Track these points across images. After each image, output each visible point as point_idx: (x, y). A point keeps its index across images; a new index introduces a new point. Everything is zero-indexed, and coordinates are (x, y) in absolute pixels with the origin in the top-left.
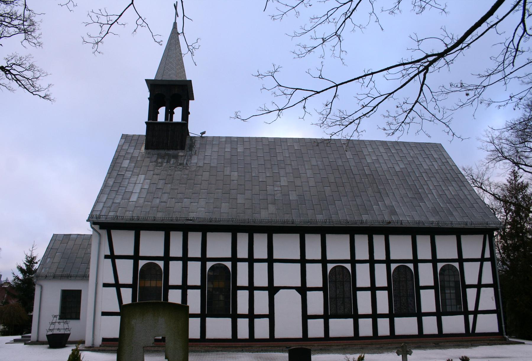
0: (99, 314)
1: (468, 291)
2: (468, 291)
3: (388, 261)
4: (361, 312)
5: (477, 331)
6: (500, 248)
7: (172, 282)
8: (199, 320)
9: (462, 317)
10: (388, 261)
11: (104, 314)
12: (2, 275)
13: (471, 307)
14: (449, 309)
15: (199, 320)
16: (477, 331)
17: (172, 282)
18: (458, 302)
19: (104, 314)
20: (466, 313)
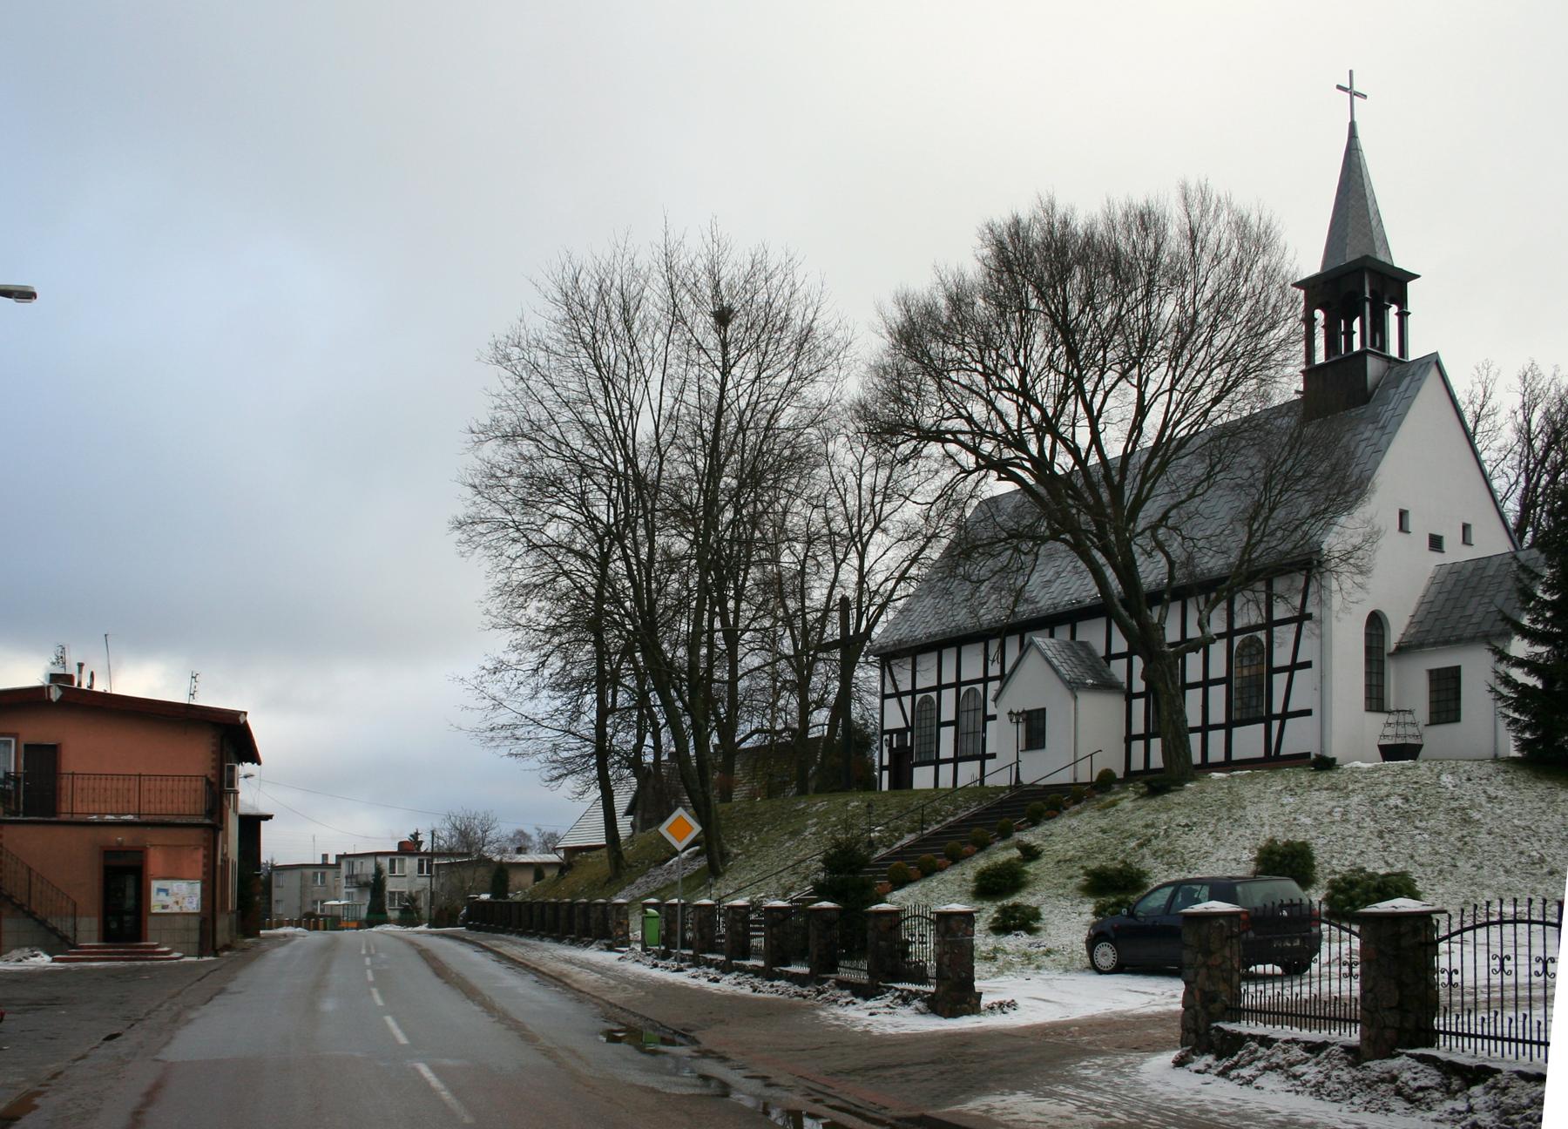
0: (1316, 712)
5: (1283, 752)
9: (1261, 726)
11: (1308, 713)
12: (1437, 353)
13: (1277, 708)
16: (1283, 752)
19: (1308, 713)
20: (1267, 719)
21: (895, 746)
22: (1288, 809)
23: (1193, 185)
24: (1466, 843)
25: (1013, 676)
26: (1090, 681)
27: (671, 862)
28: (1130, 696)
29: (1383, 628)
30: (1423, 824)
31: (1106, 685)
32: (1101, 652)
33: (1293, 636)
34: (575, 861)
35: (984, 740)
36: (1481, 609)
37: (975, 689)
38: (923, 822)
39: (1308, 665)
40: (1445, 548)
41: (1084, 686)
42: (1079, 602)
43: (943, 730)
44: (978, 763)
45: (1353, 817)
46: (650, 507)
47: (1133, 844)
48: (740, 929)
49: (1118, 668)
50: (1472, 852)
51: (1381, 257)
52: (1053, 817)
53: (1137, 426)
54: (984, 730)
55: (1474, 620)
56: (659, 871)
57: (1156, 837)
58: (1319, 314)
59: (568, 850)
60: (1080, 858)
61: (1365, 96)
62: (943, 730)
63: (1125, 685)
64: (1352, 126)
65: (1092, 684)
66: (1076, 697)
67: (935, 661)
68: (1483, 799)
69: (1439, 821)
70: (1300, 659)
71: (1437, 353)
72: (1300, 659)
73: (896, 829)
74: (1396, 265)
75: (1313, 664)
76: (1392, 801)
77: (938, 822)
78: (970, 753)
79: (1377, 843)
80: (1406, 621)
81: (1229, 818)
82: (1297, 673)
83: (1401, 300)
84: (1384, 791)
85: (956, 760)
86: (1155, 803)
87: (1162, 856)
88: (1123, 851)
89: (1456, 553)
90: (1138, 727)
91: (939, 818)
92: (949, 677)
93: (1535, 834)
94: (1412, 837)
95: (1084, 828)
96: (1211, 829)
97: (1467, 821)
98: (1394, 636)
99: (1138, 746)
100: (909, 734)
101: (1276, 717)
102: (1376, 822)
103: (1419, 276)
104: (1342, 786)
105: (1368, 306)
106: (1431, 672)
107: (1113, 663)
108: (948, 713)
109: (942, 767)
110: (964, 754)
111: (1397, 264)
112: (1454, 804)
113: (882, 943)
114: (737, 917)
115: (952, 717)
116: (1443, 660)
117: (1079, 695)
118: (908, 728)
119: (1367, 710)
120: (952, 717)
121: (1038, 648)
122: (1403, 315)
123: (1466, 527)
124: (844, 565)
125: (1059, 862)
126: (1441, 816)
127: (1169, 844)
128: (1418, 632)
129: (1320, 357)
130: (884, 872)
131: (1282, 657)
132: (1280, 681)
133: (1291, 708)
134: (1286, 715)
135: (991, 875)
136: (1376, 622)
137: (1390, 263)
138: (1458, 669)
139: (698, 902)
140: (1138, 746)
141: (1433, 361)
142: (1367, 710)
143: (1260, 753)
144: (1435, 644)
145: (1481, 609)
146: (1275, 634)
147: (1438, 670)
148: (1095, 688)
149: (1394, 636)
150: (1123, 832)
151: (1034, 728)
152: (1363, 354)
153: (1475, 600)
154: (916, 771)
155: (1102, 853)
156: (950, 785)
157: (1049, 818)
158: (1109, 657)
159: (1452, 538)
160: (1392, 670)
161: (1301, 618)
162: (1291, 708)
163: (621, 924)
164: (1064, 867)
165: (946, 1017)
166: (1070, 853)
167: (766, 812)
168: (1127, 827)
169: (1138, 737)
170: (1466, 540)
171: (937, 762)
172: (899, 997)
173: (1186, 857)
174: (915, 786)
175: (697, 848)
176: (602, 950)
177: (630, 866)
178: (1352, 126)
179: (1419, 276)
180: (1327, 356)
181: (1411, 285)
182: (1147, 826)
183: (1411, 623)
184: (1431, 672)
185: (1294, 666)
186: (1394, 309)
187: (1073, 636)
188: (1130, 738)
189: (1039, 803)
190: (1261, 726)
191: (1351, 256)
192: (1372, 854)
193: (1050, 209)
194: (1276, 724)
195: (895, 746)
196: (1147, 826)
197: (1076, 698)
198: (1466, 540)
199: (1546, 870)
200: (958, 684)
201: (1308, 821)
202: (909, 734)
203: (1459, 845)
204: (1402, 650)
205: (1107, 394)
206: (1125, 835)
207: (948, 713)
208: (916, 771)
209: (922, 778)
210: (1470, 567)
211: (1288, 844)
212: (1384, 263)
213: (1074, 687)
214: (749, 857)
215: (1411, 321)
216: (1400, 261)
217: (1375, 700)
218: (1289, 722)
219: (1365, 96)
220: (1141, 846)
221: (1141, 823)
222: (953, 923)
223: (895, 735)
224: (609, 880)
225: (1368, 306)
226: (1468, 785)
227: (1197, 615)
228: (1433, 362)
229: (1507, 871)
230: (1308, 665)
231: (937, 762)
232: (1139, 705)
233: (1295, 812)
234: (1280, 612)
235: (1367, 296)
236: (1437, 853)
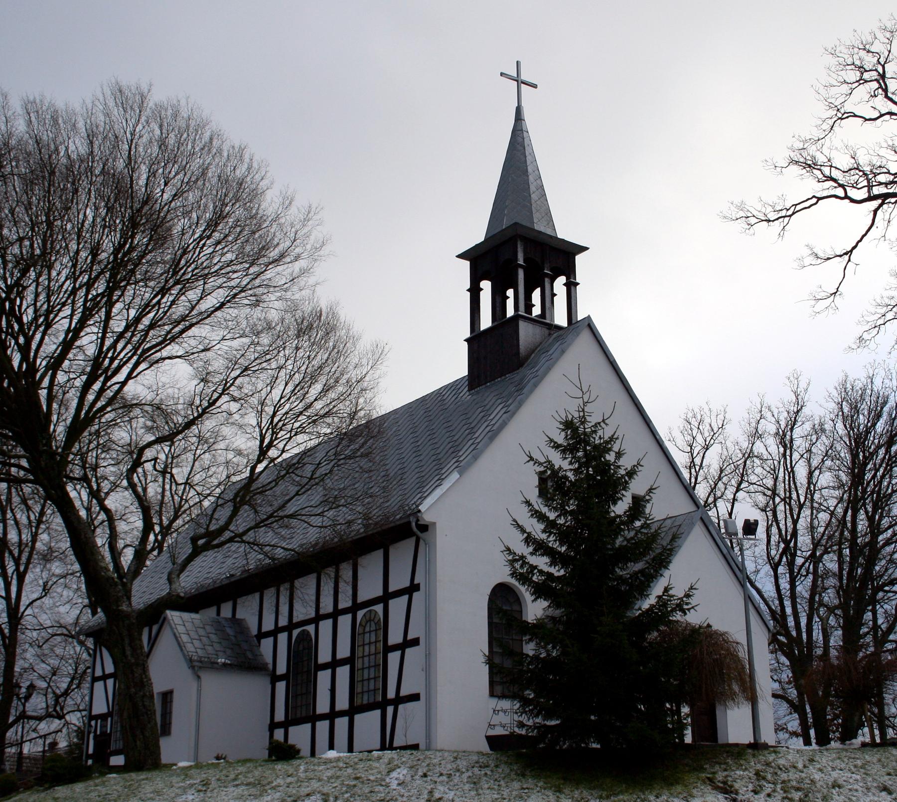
9: (378, 712)
12: (589, 317)
13: (391, 694)
21: (98, 733)
25: (153, 652)
26: (221, 660)
28: (275, 679)
29: (520, 604)
32: (254, 631)
42: (232, 576)
46: (247, 499)
51: (540, 226)
58: (486, 286)
61: (534, 86)
63: (271, 667)
64: (519, 111)
65: (224, 664)
66: (199, 677)
70: (410, 636)
71: (589, 317)
72: (410, 637)
74: (559, 236)
75: (421, 642)
83: (569, 271)
90: (280, 716)
100: (109, 719)
103: (586, 249)
105: (521, 274)
111: (560, 235)
117: (201, 674)
122: (571, 286)
124: (242, 548)
129: (486, 321)
134: (399, 700)
137: (549, 232)
152: (516, 317)
158: (261, 635)
161: (413, 588)
178: (519, 111)
179: (586, 249)
180: (494, 319)
185: (409, 643)
187: (218, 614)
191: (506, 223)
194: (390, 710)
195: (98, 733)
202: (109, 719)
212: (551, 237)
216: (565, 231)
219: (534, 86)
223: (99, 721)
225: (521, 274)
232: (281, 686)
235: (521, 262)
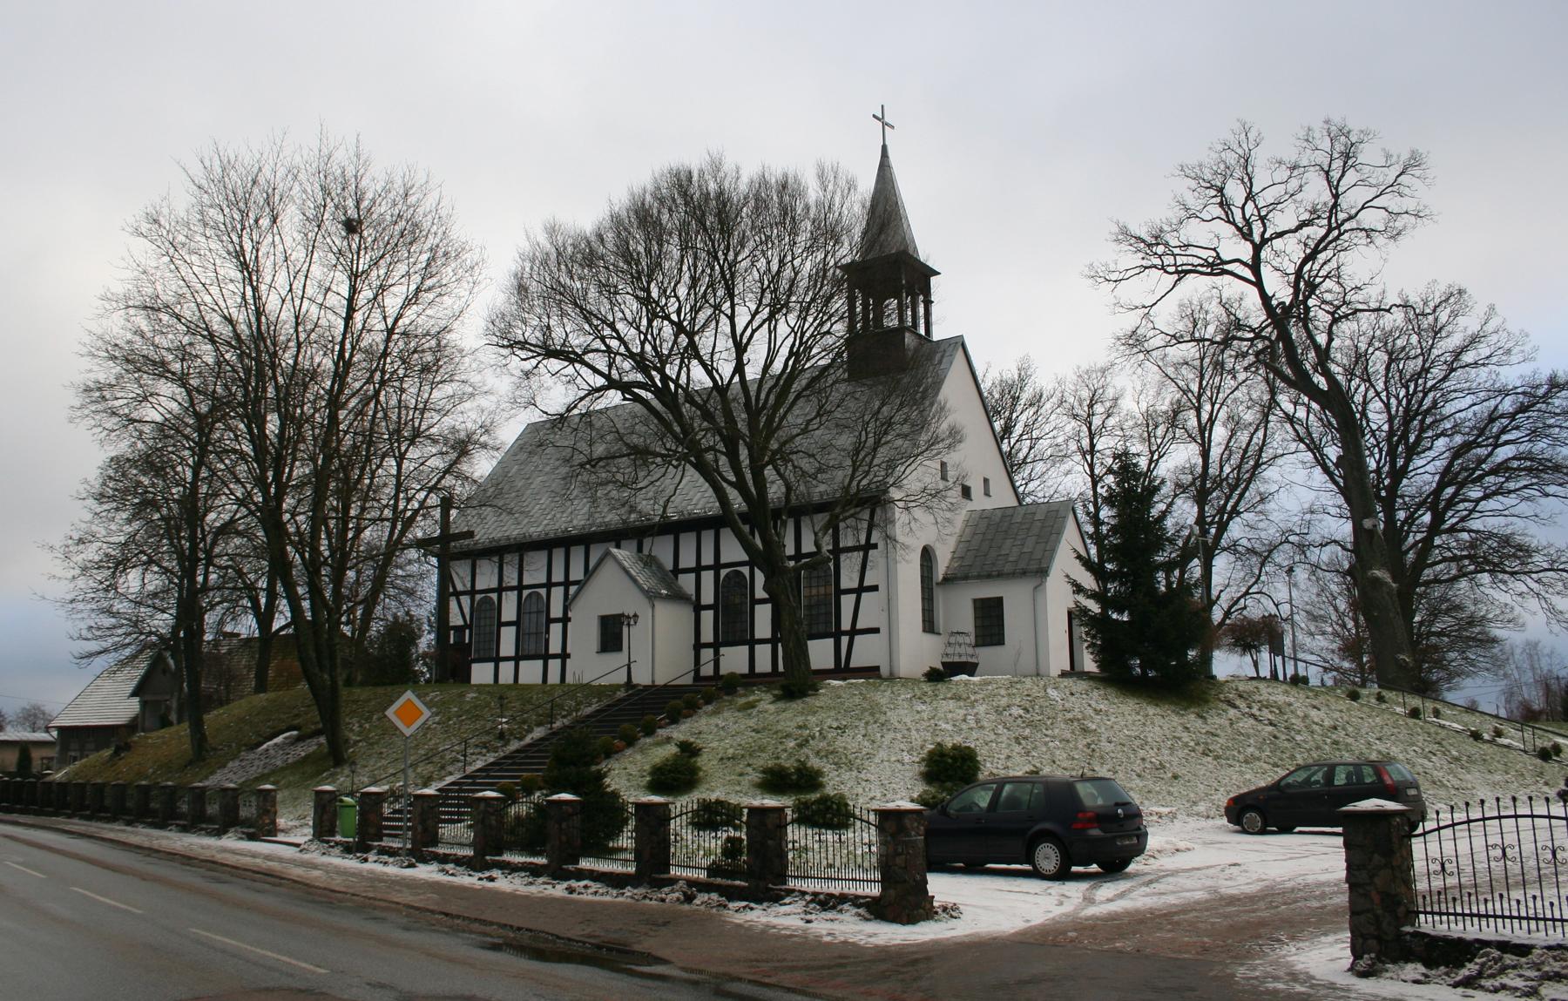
0: (884, 630)
1: (844, 598)
2: (844, 598)
3: (520, 588)
4: (758, 635)
5: (852, 665)
6: (300, 590)
7: (553, 615)
8: (769, 646)
9: (831, 641)
10: (717, 566)
11: (876, 631)
13: (846, 625)
14: (814, 630)
15: (769, 646)
16: (852, 665)
17: (553, 615)
18: (829, 622)
19: (876, 631)
20: (837, 635)
22: (925, 715)
23: (828, 166)
24: (1093, 750)
27: (265, 746)
28: (698, 608)
30: (1049, 732)
31: (677, 596)
32: (669, 566)
33: (858, 568)
34: (135, 742)
35: (547, 641)
36: (1015, 549)
37: (538, 594)
38: (551, 718)
39: (875, 588)
40: (973, 497)
41: (661, 597)
43: (503, 629)
44: (540, 663)
45: (986, 724)
47: (791, 744)
48: (494, 822)
49: (687, 582)
50: (1102, 758)
52: (691, 716)
53: (766, 367)
54: (548, 632)
55: (1011, 559)
56: (252, 756)
57: (813, 738)
59: (61, 729)
60: (743, 756)
62: (503, 629)
63: (694, 598)
64: (884, 148)
66: (653, 606)
67: (545, 561)
68: (1091, 712)
69: (1061, 730)
73: (524, 722)
76: (1016, 711)
77: (564, 717)
78: (533, 652)
79: (1017, 749)
80: (949, 556)
81: (875, 722)
82: (864, 595)
83: (927, 291)
84: (1004, 702)
85: (517, 659)
86: (797, 705)
87: (826, 756)
88: (785, 750)
89: (979, 503)
90: (707, 635)
91: (564, 713)
92: (511, 578)
93: (1147, 743)
94: (1046, 744)
95: (733, 728)
96: (863, 732)
97: (1085, 730)
98: (942, 567)
99: (707, 654)
101: (845, 633)
102: (1008, 729)
104: (965, 696)
106: (975, 601)
107: (681, 576)
108: (509, 612)
109: (502, 664)
110: (526, 653)
112: (1069, 716)
113: (770, 842)
114: (491, 810)
115: (513, 618)
116: (988, 591)
118: (466, 626)
119: (924, 631)
120: (513, 618)
121: (615, 558)
122: (928, 303)
123: (986, 481)
125: (722, 759)
126: (1063, 726)
127: (829, 745)
128: (961, 566)
130: (544, 764)
131: (849, 580)
132: (847, 602)
133: (859, 626)
134: (854, 632)
135: (670, 771)
136: (927, 555)
138: (998, 602)
139: (320, 788)
140: (707, 654)
141: (959, 343)
142: (924, 631)
143: (830, 665)
144: (979, 577)
145: (1015, 549)
146: (870, 558)
147: (982, 600)
148: (668, 598)
149: (942, 567)
150: (776, 732)
151: (612, 633)
153: (1009, 542)
154: (475, 667)
155: (762, 751)
156: (511, 681)
157: (686, 717)
158: (677, 571)
159: (977, 489)
160: (940, 597)
162: (859, 626)
163: (268, 811)
164: (729, 764)
165: (903, 923)
166: (731, 751)
167: (369, 700)
168: (780, 728)
169: (707, 645)
170: (987, 494)
171: (498, 660)
172: (812, 901)
173: (850, 757)
174: (473, 682)
175: (295, 733)
176: (241, 839)
177: (215, 749)
178: (884, 148)
181: (933, 280)
182: (800, 727)
183: (953, 558)
184: (975, 601)
185: (861, 590)
186: (921, 298)
188: (698, 646)
189: (678, 701)
190: (831, 641)
192: (1018, 759)
193: (716, 167)
194: (845, 640)
196: (800, 727)
197: (653, 607)
198: (987, 494)
199: (1170, 775)
200: (520, 588)
201: (949, 727)
203: (1089, 751)
204: (947, 580)
205: (754, 331)
206: (780, 735)
207: (509, 612)
208: (475, 667)
209: (481, 673)
210: (999, 514)
211: (955, 747)
213: (651, 596)
214: (372, 744)
215: (934, 309)
217: (929, 626)
218: (858, 638)
220: (800, 746)
221: (793, 724)
222: (907, 822)
224: (190, 763)
226: (1073, 699)
227: (813, 537)
228: (959, 343)
229: (1139, 776)
230: (875, 588)
231: (498, 660)
232: (707, 617)
233: (933, 718)
234: (847, 541)
236: (1073, 759)
